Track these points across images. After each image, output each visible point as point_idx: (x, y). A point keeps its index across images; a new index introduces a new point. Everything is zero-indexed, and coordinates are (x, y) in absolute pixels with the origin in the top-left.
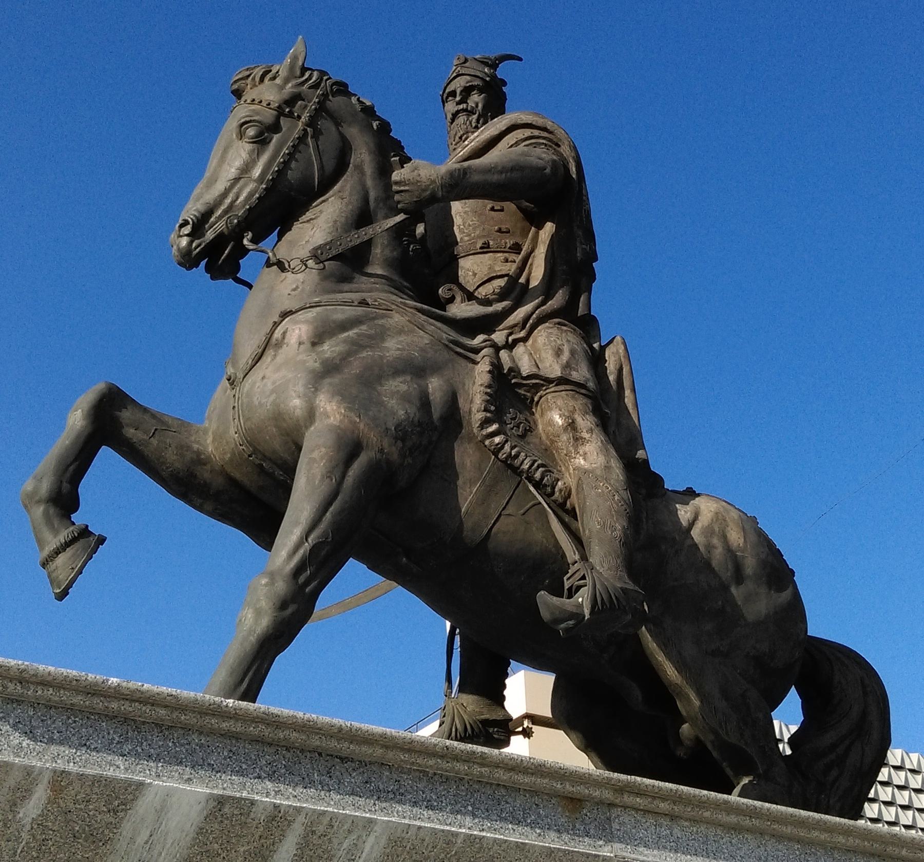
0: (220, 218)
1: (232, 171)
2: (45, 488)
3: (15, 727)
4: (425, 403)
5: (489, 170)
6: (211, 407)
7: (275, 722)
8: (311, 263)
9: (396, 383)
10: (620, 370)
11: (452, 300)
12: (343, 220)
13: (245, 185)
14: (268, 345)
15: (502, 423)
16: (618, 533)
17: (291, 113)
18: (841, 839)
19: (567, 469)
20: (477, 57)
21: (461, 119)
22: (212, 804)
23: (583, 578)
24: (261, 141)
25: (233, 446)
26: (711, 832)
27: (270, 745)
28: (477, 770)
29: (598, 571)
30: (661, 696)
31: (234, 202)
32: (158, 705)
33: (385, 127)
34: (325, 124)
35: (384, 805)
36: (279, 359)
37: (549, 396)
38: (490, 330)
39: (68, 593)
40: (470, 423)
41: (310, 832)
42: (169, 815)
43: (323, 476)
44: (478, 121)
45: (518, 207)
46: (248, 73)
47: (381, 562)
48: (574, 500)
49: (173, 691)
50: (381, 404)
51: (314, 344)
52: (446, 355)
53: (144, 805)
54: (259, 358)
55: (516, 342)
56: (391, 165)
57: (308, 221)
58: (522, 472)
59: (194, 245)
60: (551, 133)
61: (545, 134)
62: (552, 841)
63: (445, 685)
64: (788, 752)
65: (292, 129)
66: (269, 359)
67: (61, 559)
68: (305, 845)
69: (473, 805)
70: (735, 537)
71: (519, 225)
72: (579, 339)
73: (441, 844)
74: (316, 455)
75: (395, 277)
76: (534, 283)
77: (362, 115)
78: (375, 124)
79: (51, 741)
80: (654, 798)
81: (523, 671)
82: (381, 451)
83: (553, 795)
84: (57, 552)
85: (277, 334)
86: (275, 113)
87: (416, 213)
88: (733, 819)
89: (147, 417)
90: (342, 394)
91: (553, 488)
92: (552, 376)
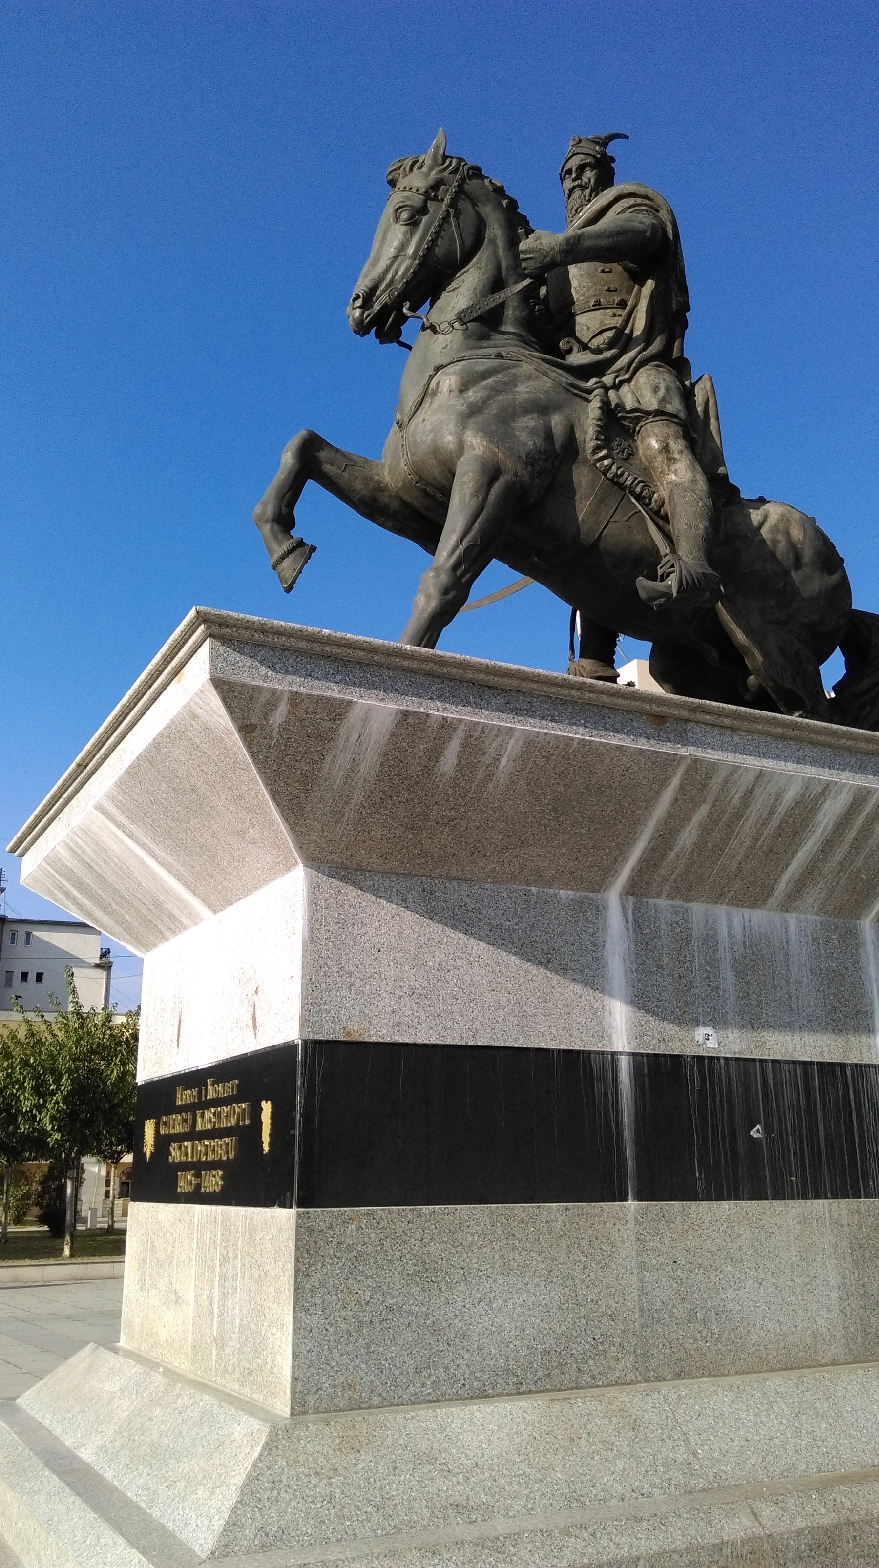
1: (390, 251)
2: (270, 510)
3: (261, 663)
4: (549, 435)
5: (599, 236)
6: (385, 448)
7: (441, 661)
8: (456, 325)
9: (526, 420)
10: (707, 403)
11: (570, 351)
12: (481, 287)
13: (403, 261)
14: (426, 394)
15: (610, 449)
16: (701, 532)
17: (436, 196)
18: (863, 745)
19: (662, 484)
20: (590, 137)
21: (577, 193)
23: (673, 566)
24: (413, 223)
25: (403, 476)
26: (763, 739)
27: (438, 677)
28: (587, 695)
29: (684, 561)
30: (733, 655)
31: (393, 277)
32: (358, 649)
35: (520, 718)
36: (435, 405)
37: (648, 426)
38: (601, 374)
39: (293, 588)
40: (584, 450)
41: (468, 736)
42: (371, 723)
43: (471, 495)
44: (590, 195)
46: (399, 164)
47: (520, 561)
48: (667, 507)
49: (368, 639)
51: (461, 391)
52: (565, 396)
53: (354, 715)
54: (420, 405)
55: (622, 383)
56: (518, 236)
57: (453, 290)
58: (626, 487)
59: (365, 315)
61: (646, 202)
62: (642, 744)
63: (569, 653)
64: (833, 695)
65: (437, 210)
66: (428, 405)
67: (286, 563)
68: (465, 744)
69: (585, 719)
70: (797, 533)
71: (625, 284)
72: (673, 378)
73: (562, 745)
74: (465, 479)
76: (637, 333)
77: (493, 194)
79: (287, 672)
81: (636, 660)
82: (515, 474)
83: (643, 713)
84: (283, 558)
85: (433, 385)
86: (423, 197)
87: (539, 279)
88: (779, 730)
89: (339, 456)
91: (650, 499)
92: (651, 409)
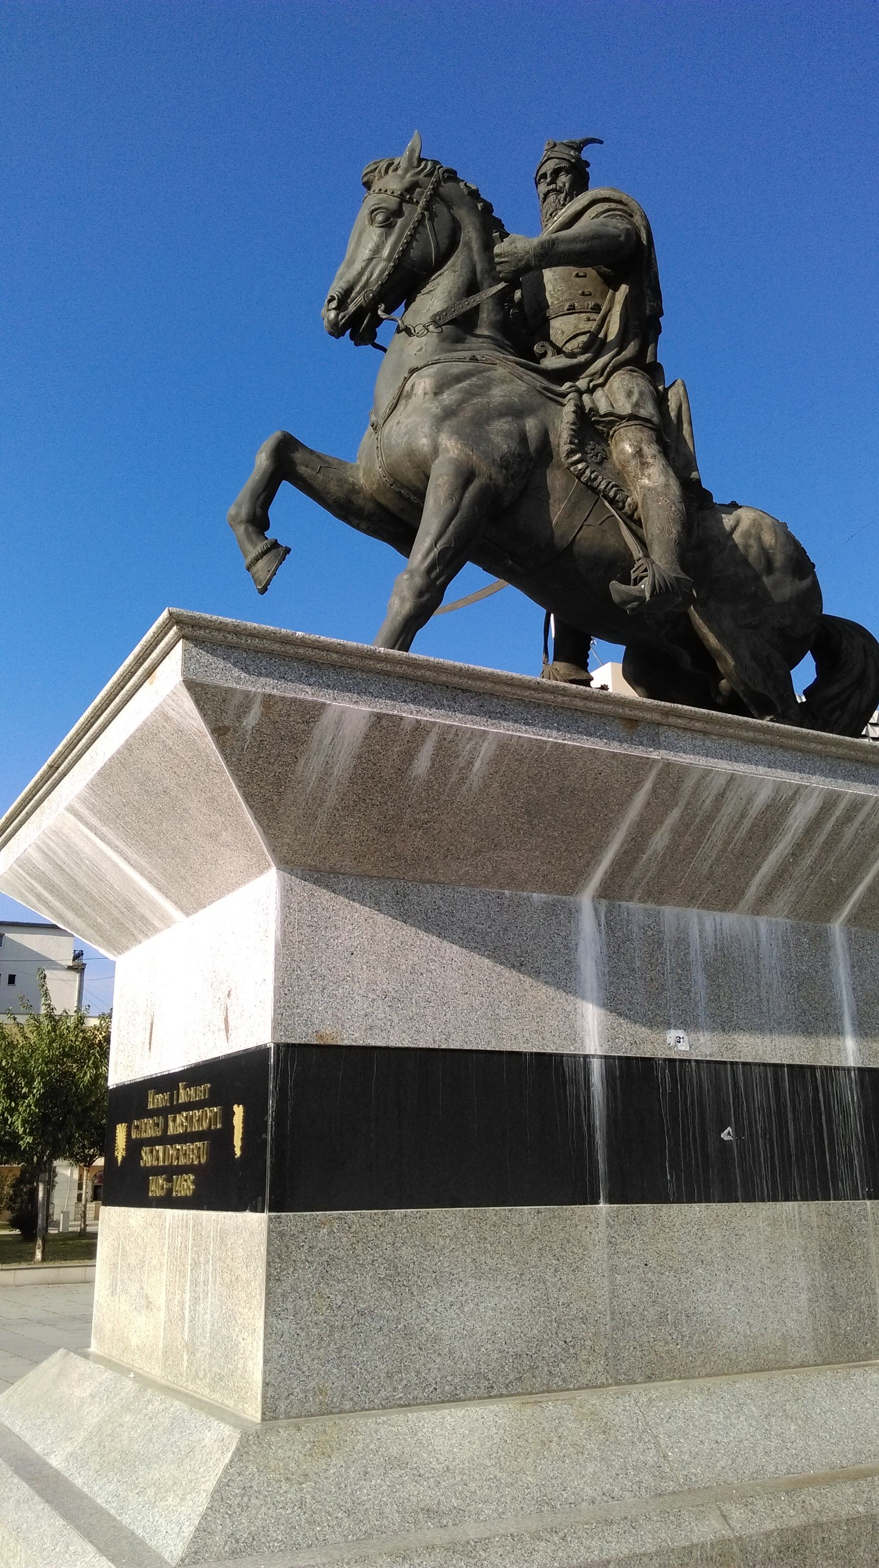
0: (359, 293)
1: (366, 253)
2: (244, 512)
3: (235, 664)
4: (523, 438)
5: (574, 240)
6: (361, 447)
7: (415, 664)
8: (431, 328)
9: (500, 423)
10: (680, 408)
11: (544, 355)
13: (378, 264)
14: (401, 397)
15: (584, 453)
17: (411, 199)
18: (833, 749)
19: (635, 488)
21: (552, 198)
22: (374, 719)
23: (646, 570)
24: (387, 225)
27: (412, 680)
28: (560, 699)
29: (657, 565)
30: (705, 659)
31: (368, 279)
33: (488, 208)
34: (439, 208)
35: (494, 721)
36: (410, 408)
37: (622, 430)
40: (558, 454)
41: (442, 739)
42: (345, 726)
43: (446, 499)
44: (565, 200)
45: (599, 274)
46: (375, 166)
49: (341, 641)
50: (488, 440)
51: (436, 394)
52: (539, 400)
53: (327, 719)
55: (596, 387)
58: (600, 491)
59: (340, 317)
60: (626, 205)
62: (615, 748)
63: (543, 656)
66: (402, 408)
67: (260, 564)
68: (439, 747)
69: (558, 723)
70: (768, 539)
73: (535, 748)
75: (499, 337)
76: (611, 337)
77: (468, 198)
78: (480, 206)
79: (260, 674)
80: (692, 719)
81: (610, 663)
82: (490, 477)
83: (616, 716)
84: (257, 559)
85: (408, 387)
88: (751, 734)
89: (313, 457)
90: (459, 434)
91: (624, 503)
92: (625, 413)
